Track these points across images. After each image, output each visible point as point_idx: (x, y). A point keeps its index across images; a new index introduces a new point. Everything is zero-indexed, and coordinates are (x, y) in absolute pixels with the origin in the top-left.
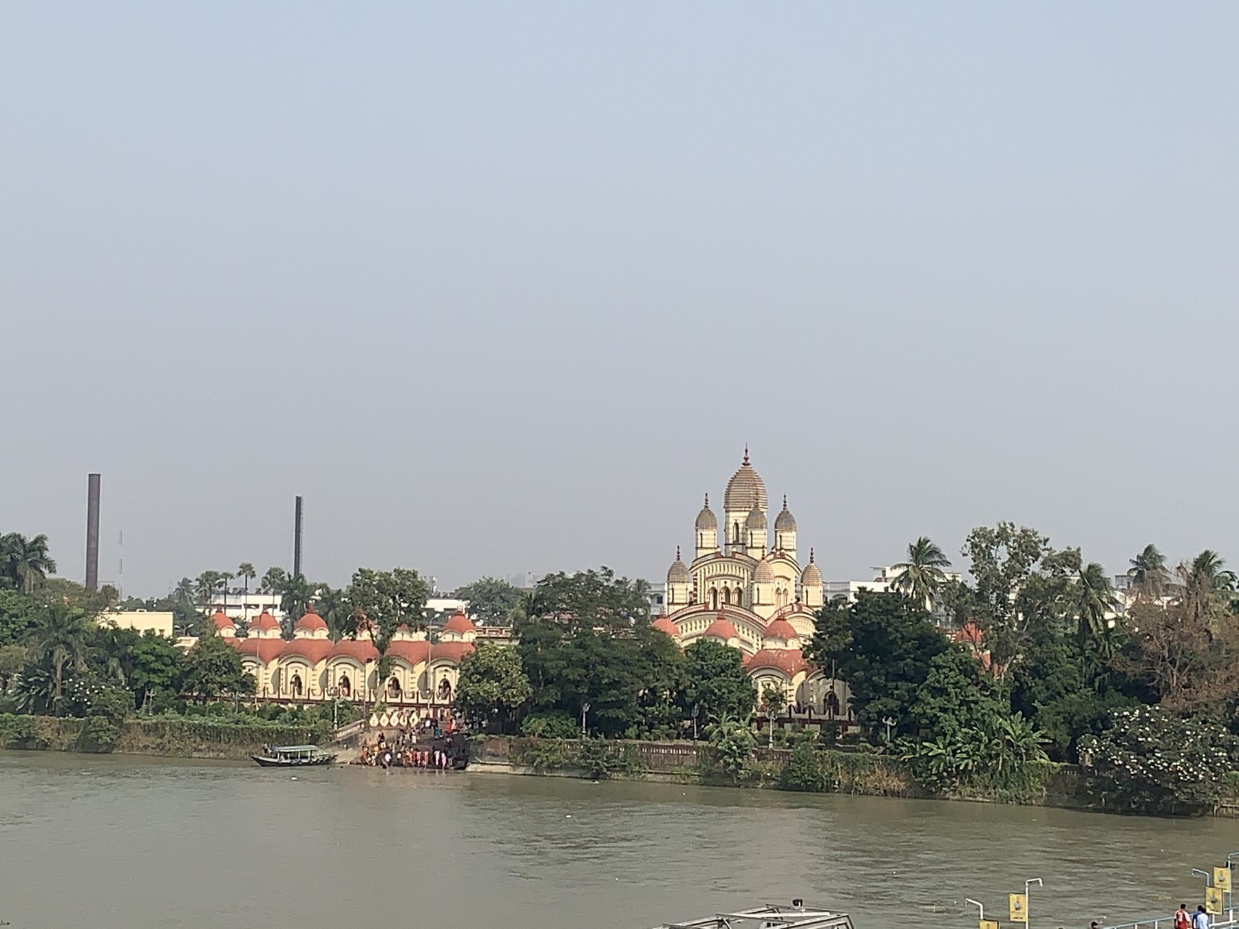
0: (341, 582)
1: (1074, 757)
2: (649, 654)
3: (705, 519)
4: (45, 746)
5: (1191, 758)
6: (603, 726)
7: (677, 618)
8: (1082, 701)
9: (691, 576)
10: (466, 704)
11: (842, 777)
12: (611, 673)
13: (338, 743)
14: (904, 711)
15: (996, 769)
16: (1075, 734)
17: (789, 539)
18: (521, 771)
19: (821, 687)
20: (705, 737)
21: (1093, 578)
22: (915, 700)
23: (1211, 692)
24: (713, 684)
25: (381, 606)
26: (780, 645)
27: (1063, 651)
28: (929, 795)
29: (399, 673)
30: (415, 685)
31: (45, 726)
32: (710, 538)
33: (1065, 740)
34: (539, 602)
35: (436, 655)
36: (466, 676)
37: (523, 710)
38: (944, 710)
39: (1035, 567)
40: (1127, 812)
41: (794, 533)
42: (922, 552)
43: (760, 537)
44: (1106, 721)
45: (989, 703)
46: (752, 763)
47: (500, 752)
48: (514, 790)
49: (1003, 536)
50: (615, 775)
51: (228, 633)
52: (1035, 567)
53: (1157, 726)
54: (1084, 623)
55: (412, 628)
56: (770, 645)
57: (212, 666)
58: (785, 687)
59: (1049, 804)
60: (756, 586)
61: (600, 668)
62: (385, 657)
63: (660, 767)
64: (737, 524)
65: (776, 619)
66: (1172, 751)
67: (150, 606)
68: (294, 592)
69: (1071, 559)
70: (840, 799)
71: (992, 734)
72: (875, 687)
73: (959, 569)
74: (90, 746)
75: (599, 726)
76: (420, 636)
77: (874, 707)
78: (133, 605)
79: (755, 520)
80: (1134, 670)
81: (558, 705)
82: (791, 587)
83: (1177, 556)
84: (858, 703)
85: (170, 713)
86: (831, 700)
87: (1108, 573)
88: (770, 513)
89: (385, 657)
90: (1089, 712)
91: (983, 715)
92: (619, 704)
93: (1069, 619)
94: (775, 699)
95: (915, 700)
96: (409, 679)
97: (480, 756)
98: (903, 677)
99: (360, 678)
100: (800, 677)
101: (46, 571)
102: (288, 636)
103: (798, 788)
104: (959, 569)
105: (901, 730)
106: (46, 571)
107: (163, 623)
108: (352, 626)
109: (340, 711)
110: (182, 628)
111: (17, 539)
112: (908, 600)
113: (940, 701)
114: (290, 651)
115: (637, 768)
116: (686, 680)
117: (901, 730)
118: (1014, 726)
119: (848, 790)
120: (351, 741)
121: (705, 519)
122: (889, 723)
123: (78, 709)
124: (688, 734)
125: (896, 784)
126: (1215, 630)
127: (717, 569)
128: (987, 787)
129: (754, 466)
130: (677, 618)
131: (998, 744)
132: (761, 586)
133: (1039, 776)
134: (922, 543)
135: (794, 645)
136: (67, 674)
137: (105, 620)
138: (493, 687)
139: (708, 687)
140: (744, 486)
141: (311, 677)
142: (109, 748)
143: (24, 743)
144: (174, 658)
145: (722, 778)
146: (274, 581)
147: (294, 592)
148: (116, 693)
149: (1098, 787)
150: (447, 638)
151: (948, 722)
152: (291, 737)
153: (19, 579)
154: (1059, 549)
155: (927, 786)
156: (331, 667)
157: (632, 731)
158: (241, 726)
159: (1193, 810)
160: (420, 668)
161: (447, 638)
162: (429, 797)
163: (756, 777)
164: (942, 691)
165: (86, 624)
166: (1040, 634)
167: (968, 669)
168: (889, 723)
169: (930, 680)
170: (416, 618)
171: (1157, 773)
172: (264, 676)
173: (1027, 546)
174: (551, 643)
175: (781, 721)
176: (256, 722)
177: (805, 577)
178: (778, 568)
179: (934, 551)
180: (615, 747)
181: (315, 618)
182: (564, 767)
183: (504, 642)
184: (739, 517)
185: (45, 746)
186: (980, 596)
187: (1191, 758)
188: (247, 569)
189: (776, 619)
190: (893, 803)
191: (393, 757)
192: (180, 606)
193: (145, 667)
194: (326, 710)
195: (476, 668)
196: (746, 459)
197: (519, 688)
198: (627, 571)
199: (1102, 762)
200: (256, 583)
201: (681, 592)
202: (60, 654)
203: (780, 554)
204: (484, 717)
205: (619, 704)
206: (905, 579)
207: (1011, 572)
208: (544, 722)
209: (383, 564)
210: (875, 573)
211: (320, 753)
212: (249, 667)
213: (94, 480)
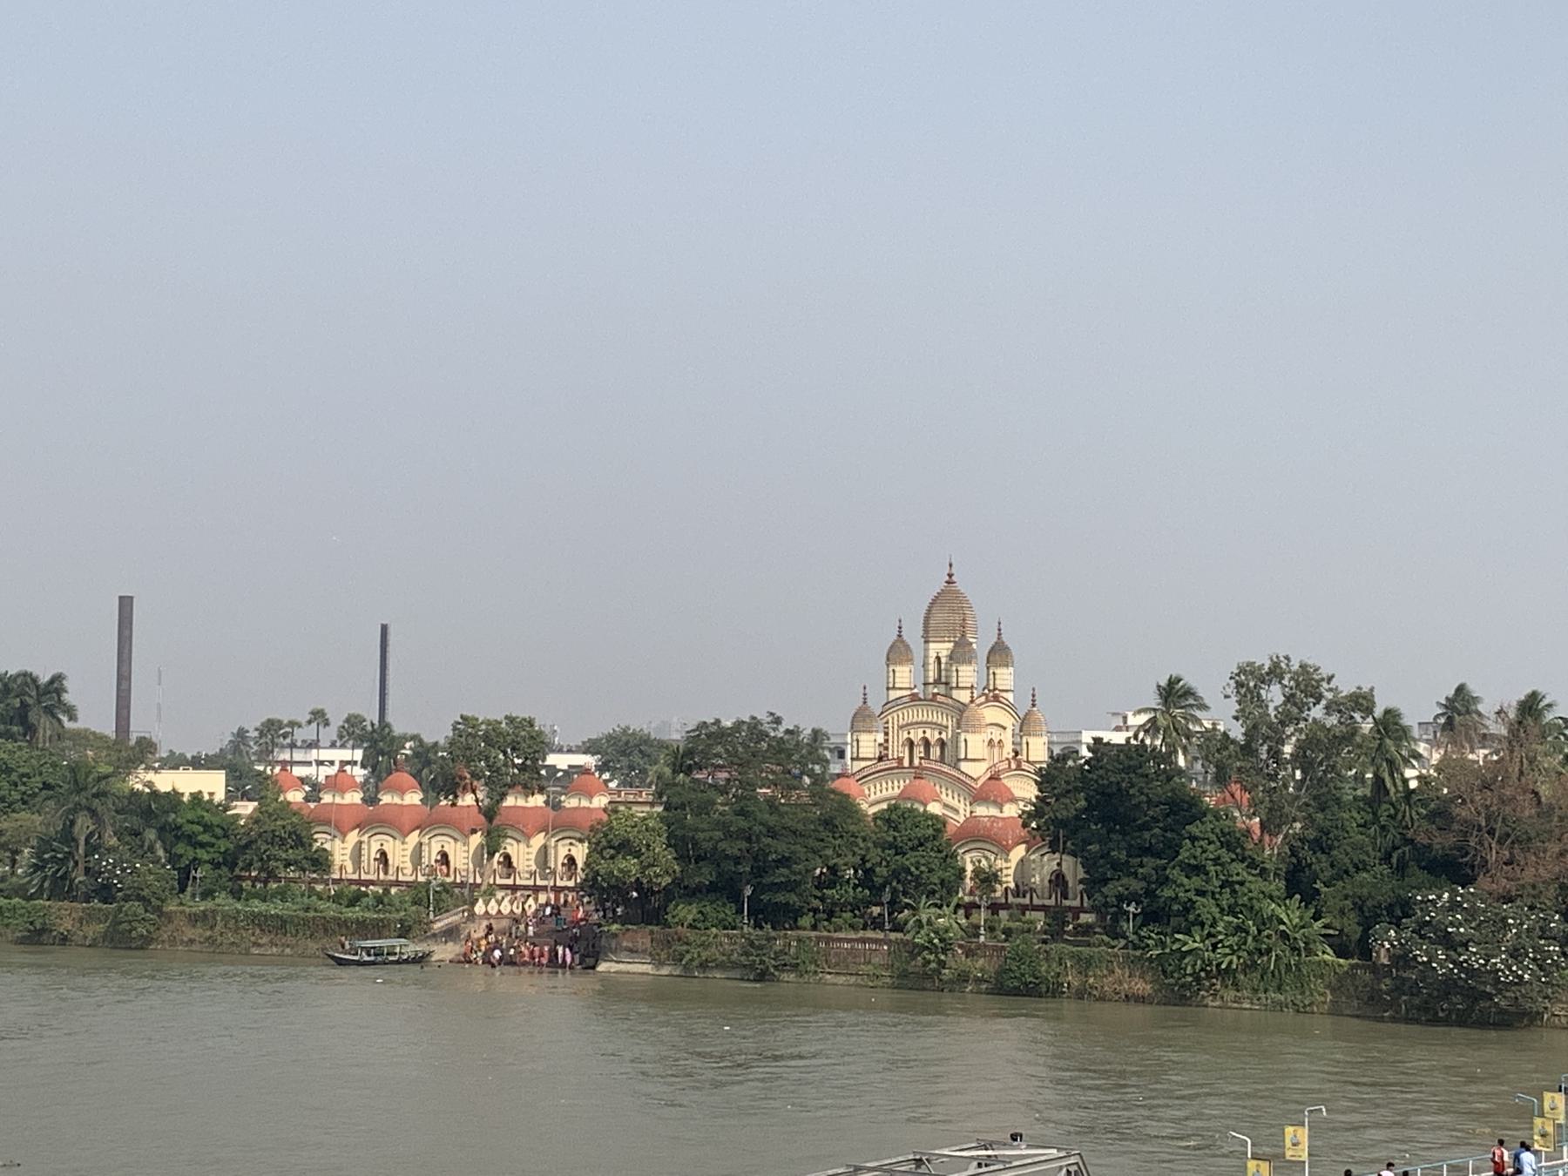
1: (1365, 952)
2: (828, 823)
4: (64, 940)
6: (770, 914)
7: (863, 777)
8: (1375, 882)
9: (881, 724)
10: (593, 886)
12: (780, 847)
13: (434, 935)
14: (1149, 893)
15: (1264, 967)
16: (1367, 925)
17: (1005, 677)
18: (665, 971)
19: (1046, 865)
20: (898, 928)
21: (1390, 725)
22: (1165, 881)
24: (909, 860)
25: (487, 763)
26: (993, 811)
27: (1352, 819)
28: (1183, 1001)
29: (511, 847)
30: (532, 863)
31: (65, 916)
32: (904, 676)
33: (1355, 932)
35: (559, 824)
36: (596, 850)
39: (1317, 712)
40: (1435, 1021)
41: (1011, 669)
42: (1174, 693)
43: (967, 674)
45: (1256, 885)
46: (958, 960)
47: (640, 947)
48: (656, 995)
49: (1275, 672)
50: (785, 977)
51: (295, 796)
52: (1317, 712)
53: (1471, 914)
54: (1379, 782)
55: (528, 791)
56: (981, 811)
58: (1000, 864)
59: (1335, 1011)
60: (963, 736)
63: (842, 965)
64: (938, 658)
65: (988, 776)
66: (1490, 947)
67: (197, 763)
68: (379, 746)
69: (1362, 702)
70: (1069, 1006)
71: (1263, 923)
72: (1116, 866)
73: (1221, 715)
76: (538, 800)
79: (961, 653)
80: (1442, 842)
81: (713, 888)
82: (1007, 738)
83: (1496, 698)
84: (1093, 883)
85: (223, 901)
86: (1058, 880)
87: (1410, 720)
88: (981, 644)
91: (1250, 899)
92: (790, 886)
93: (1359, 778)
94: (987, 879)
95: (1165, 881)
96: (523, 854)
97: (614, 952)
98: (1148, 851)
99: (462, 854)
100: (1019, 852)
101: (65, 719)
102: (370, 800)
103: (1016, 992)
104: (1221, 715)
106: (65, 719)
107: (213, 784)
110: (237, 790)
112: (1155, 754)
113: (1197, 882)
114: (373, 820)
115: (813, 967)
116: (874, 855)
117: (1152, 916)
118: (1290, 914)
119: (1080, 995)
120: (451, 933)
121: (898, 652)
122: (1131, 909)
123: (105, 893)
124: (877, 924)
125: (1141, 987)
126: (1545, 791)
128: (1255, 991)
129: (960, 585)
130: (863, 777)
131: (1270, 937)
132: (969, 737)
133: (1322, 976)
134: (1173, 682)
135: (1011, 811)
136: (91, 849)
137: (140, 780)
138: (631, 865)
139: (902, 865)
141: (400, 852)
142: (145, 942)
143: (37, 936)
144: (227, 828)
145: (921, 979)
146: (353, 731)
147: (379, 746)
148: (154, 871)
149: (1397, 990)
153: (30, 729)
155: (1180, 989)
156: (425, 840)
157: (806, 921)
158: (311, 914)
160: (538, 840)
162: (551, 1005)
163: (963, 978)
164: (1198, 869)
165: (116, 786)
166: (1323, 798)
167: (1232, 841)
168: (1131, 909)
170: (533, 777)
171: (1471, 972)
172: (340, 851)
173: (1307, 685)
174: (704, 808)
175: (994, 908)
176: (330, 910)
177: (1025, 725)
178: (991, 714)
179: (1189, 693)
180: (784, 940)
181: (405, 778)
182: (721, 966)
183: (644, 807)
184: (942, 648)
186: (1248, 749)
187: (1516, 954)
188: (319, 716)
189: (988, 776)
191: (503, 954)
195: (609, 841)
196: (950, 576)
197: (664, 866)
198: (801, 718)
199: (1402, 959)
200: (330, 733)
201: (869, 744)
202: (84, 824)
203: (994, 697)
204: (620, 901)
205: (790, 886)
206: (1152, 727)
207: (1286, 719)
209: (491, 710)
211: (411, 948)
212: (322, 840)
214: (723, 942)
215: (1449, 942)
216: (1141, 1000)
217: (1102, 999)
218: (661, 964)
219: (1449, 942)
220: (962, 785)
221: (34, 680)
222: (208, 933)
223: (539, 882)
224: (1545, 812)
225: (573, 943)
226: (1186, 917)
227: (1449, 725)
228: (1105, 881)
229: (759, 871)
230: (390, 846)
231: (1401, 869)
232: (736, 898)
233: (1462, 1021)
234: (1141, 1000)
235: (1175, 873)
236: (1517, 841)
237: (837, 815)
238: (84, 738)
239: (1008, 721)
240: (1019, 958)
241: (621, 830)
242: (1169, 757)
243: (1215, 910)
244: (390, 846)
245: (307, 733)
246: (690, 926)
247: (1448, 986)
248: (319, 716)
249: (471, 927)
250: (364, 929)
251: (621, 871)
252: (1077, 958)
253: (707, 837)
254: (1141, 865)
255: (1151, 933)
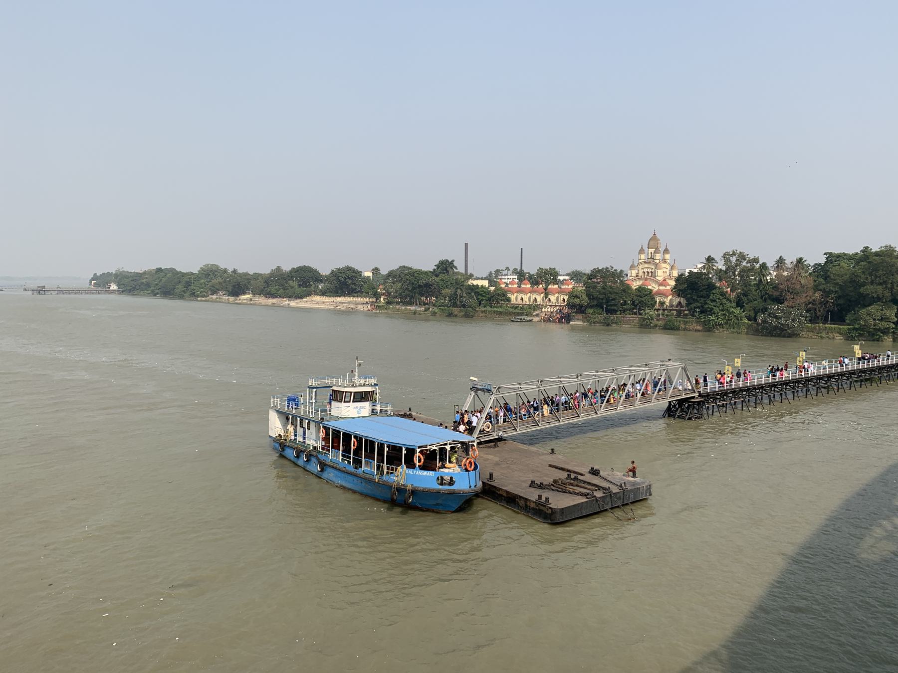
0: (533, 271)
1: (755, 320)
2: (624, 291)
3: (641, 251)
4: (456, 316)
5: (793, 320)
7: (632, 280)
8: (758, 303)
10: (570, 305)
11: (682, 326)
12: (613, 296)
15: (730, 323)
16: (756, 313)
17: (668, 257)
19: (676, 300)
20: (640, 314)
21: (764, 266)
22: (706, 303)
23: (801, 300)
24: (643, 299)
25: (545, 278)
27: (753, 289)
28: (709, 331)
29: (550, 297)
31: (456, 311)
32: (643, 257)
33: (753, 315)
34: (591, 276)
35: (561, 292)
36: (570, 297)
37: (586, 307)
39: (744, 264)
40: (772, 336)
42: (710, 260)
43: (658, 256)
44: (766, 309)
45: (729, 304)
46: (655, 322)
48: (582, 329)
49: (734, 254)
51: (503, 286)
52: (744, 264)
53: (783, 310)
54: (760, 281)
55: (554, 284)
56: (661, 288)
57: (499, 295)
62: (547, 293)
63: (627, 323)
65: (663, 280)
66: (787, 319)
67: (482, 279)
68: (521, 275)
69: (756, 260)
70: (682, 332)
71: (730, 313)
72: (694, 300)
73: (721, 265)
74: (467, 316)
75: (608, 311)
76: (556, 286)
77: (693, 306)
78: (477, 279)
79: (657, 251)
80: (776, 294)
81: (597, 305)
82: (668, 271)
83: (790, 259)
84: (687, 305)
85: (488, 308)
86: (680, 303)
87: (769, 265)
88: (662, 249)
89: (547, 293)
90: (761, 306)
92: (615, 305)
93: (755, 279)
94: (662, 303)
95: (706, 303)
96: (553, 298)
98: (702, 297)
99: (539, 298)
100: (670, 297)
102: (519, 286)
104: (721, 265)
105: (702, 312)
107: (485, 283)
108: (537, 283)
109: (535, 307)
110: (490, 285)
111: (447, 261)
112: (705, 274)
114: (520, 291)
116: (635, 298)
117: (702, 312)
118: (737, 311)
119: (685, 329)
120: (537, 315)
121: (641, 251)
123: (464, 306)
124: (635, 314)
125: (699, 328)
126: (803, 282)
127: (643, 266)
130: (632, 280)
131: (732, 316)
134: (801, 259)
135: (668, 288)
136: (461, 297)
137: (471, 282)
138: (577, 300)
139: (642, 300)
140: (654, 241)
141: (526, 298)
142: (472, 317)
143: (450, 315)
144: (489, 292)
145: (646, 326)
146: (515, 272)
147: (521, 275)
148: (474, 302)
149: (763, 329)
151: (716, 310)
152: (521, 313)
153: (448, 272)
154: (752, 257)
155: (709, 328)
159: (793, 335)
160: (557, 295)
162: (559, 331)
163: (656, 326)
164: (715, 301)
165: (465, 283)
166: (746, 284)
167: (723, 294)
170: (555, 281)
171: (782, 324)
172: (513, 297)
173: (742, 257)
174: (595, 288)
175: (664, 310)
176: (511, 310)
177: (672, 268)
178: (664, 265)
179: (713, 259)
180: (614, 317)
181: (526, 281)
183: (581, 287)
184: (652, 250)
186: (726, 272)
187: (793, 320)
188: (507, 269)
189: (663, 280)
190: (699, 333)
191: (548, 320)
192: (489, 278)
193: (481, 295)
194: (530, 307)
195: (572, 295)
197: (585, 300)
198: (618, 268)
199: (764, 321)
200: (510, 272)
201: (634, 273)
202: (459, 291)
203: (665, 261)
204: (575, 308)
205: (615, 305)
206: (704, 267)
207: (737, 265)
209: (546, 266)
210: (696, 265)
211: (528, 318)
212: (509, 295)
213: (466, 245)
214: (599, 318)
215: (776, 317)
216: (699, 331)
219: (776, 317)
220: (657, 282)
221: (820, 265)
224: (802, 287)
225: (565, 318)
226: (711, 312)
227: (778, 267)
229: (607, 302)
230: (524, 296)
231: (765, 300)
232: (602, 308)
233: (779, 336)
234: (699, 331)
235: (709, 302)
236: (795, 293)
237: (626, 289)
238: (458, 273)
239: (668, 267)
240: (670, 321)
241: (575, 293)
242: (708, 275)
244: (524, 296)
245: (504, 273)
247: (776, 327)
248: (507, 269)
250: (518, 314)
253: (596, 294)
255: (702, 316)
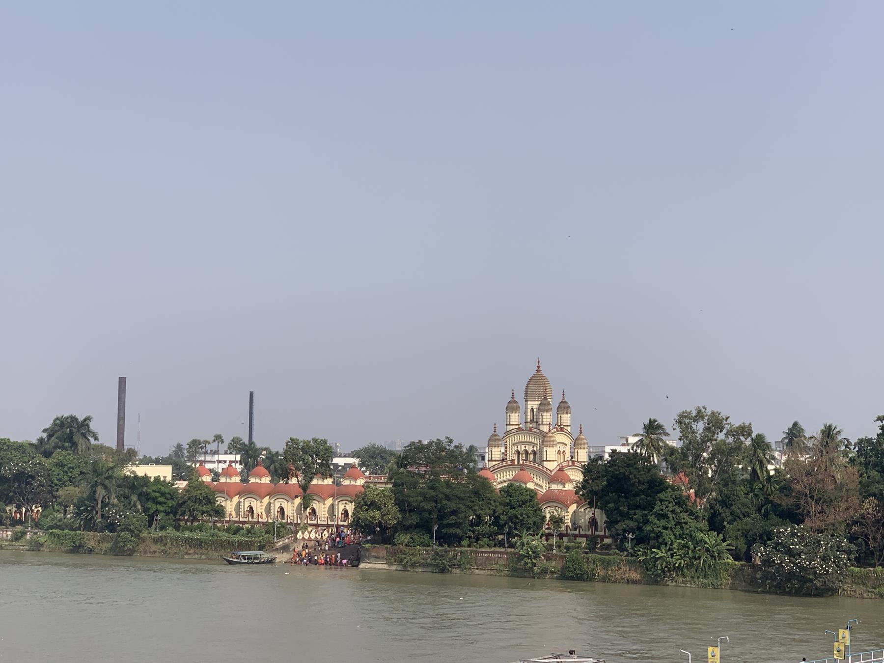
6: (445, 539)
9: (503, 443)
11: (600, 572)
13: (277, 549)
14: (639, 528)
15: (698, 565)
18: (394, 567)
31: (91, 539)
38: (665, 528)
46: (542, 562)
49: (700, 415)
50: (454, 571)
58: (563, 513)
59: (733, 588)
61: (445, 502)
64: (532, 409)
77: (620, 526)
88: (554, 401)
98: (638, 507)
99: (291, 508)
103: (571, 578)
113: (663, 522)
119: (604, 579)
120: (285, 548)
122: (630, 536)
125: (635, 576)
128: (693, 578)
129: (543, 372)
132: (548, 449)
138: (376, 514)
140: (537, 384)
150: (346, 482)
151: (668, 536)
156: (272, 501)
161: (346, 482)
168: (630, 536)
169: (657, 508)
182: (422, 565)
185: (91, 551)
196: (539, 367)
208: (408, 536)
216: (634, 582)
217: (615, 582)
218: (391, 564)
222: (163, 548)
223: (330, 523)
228: (617, 522)
234: (634, 582)
243: (673, 537)
246: (406, 545)
249: (295, 545)
251: (371, 517)
252: (603, 561)
254: (635, 514)
